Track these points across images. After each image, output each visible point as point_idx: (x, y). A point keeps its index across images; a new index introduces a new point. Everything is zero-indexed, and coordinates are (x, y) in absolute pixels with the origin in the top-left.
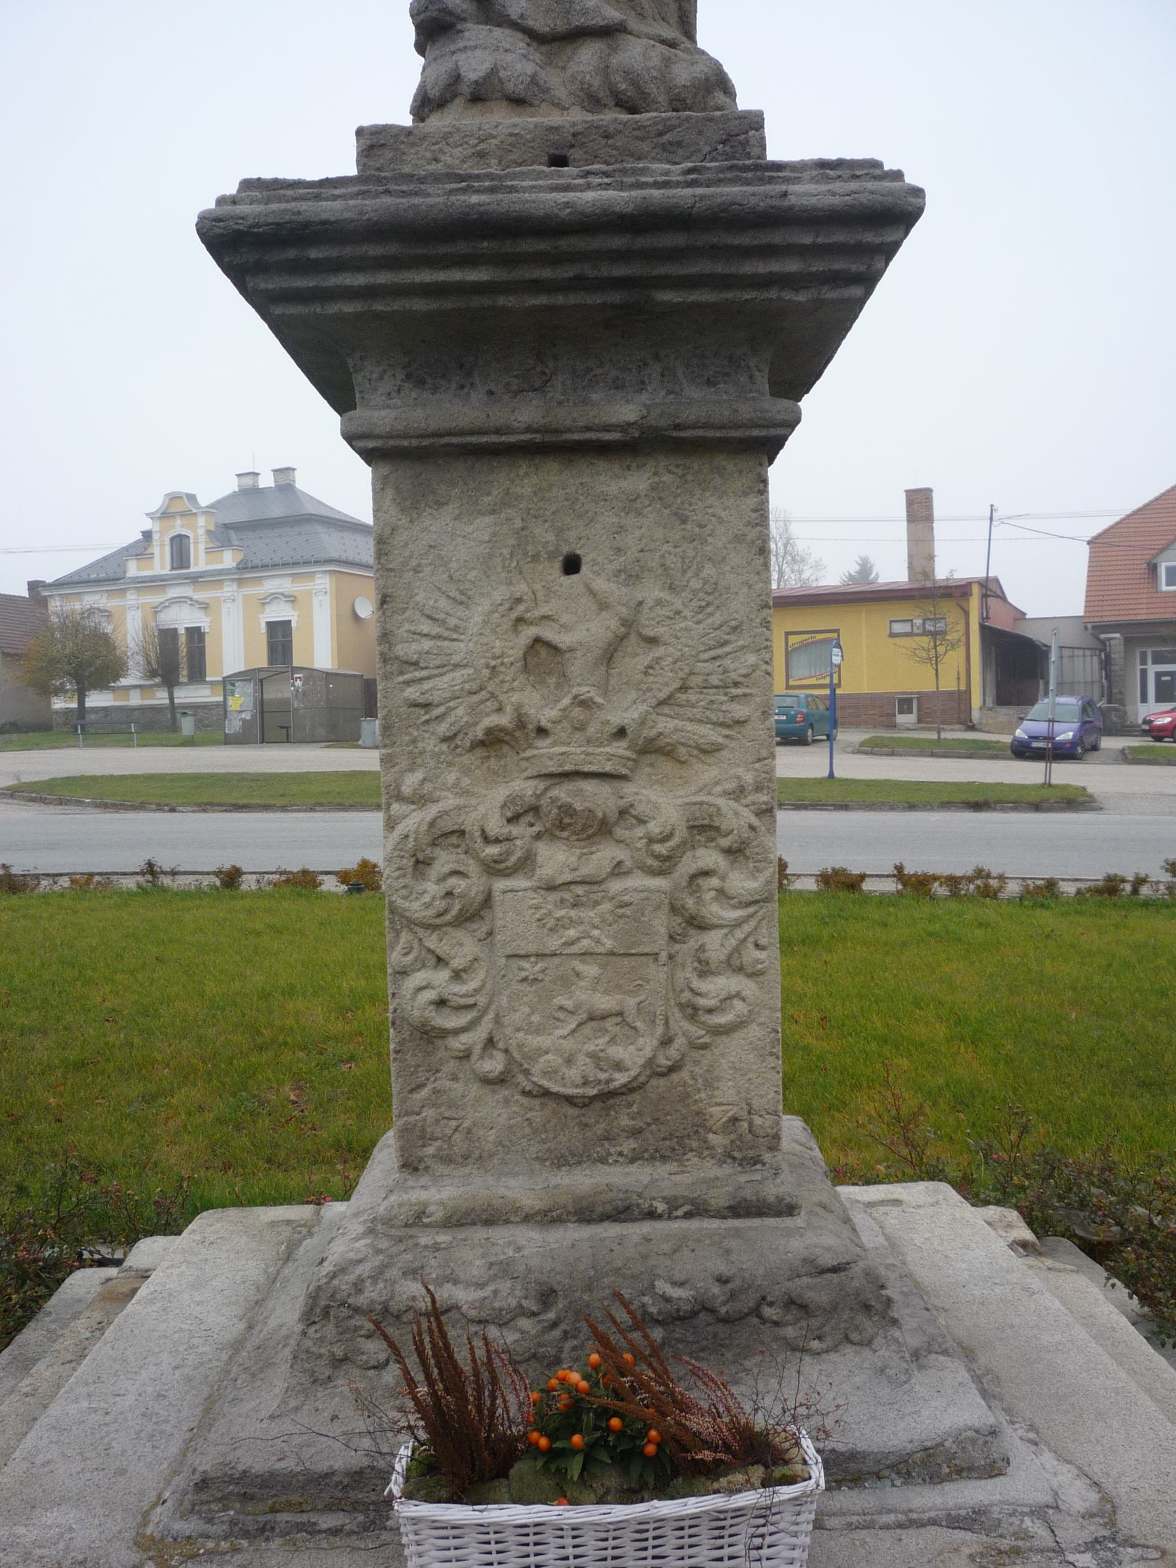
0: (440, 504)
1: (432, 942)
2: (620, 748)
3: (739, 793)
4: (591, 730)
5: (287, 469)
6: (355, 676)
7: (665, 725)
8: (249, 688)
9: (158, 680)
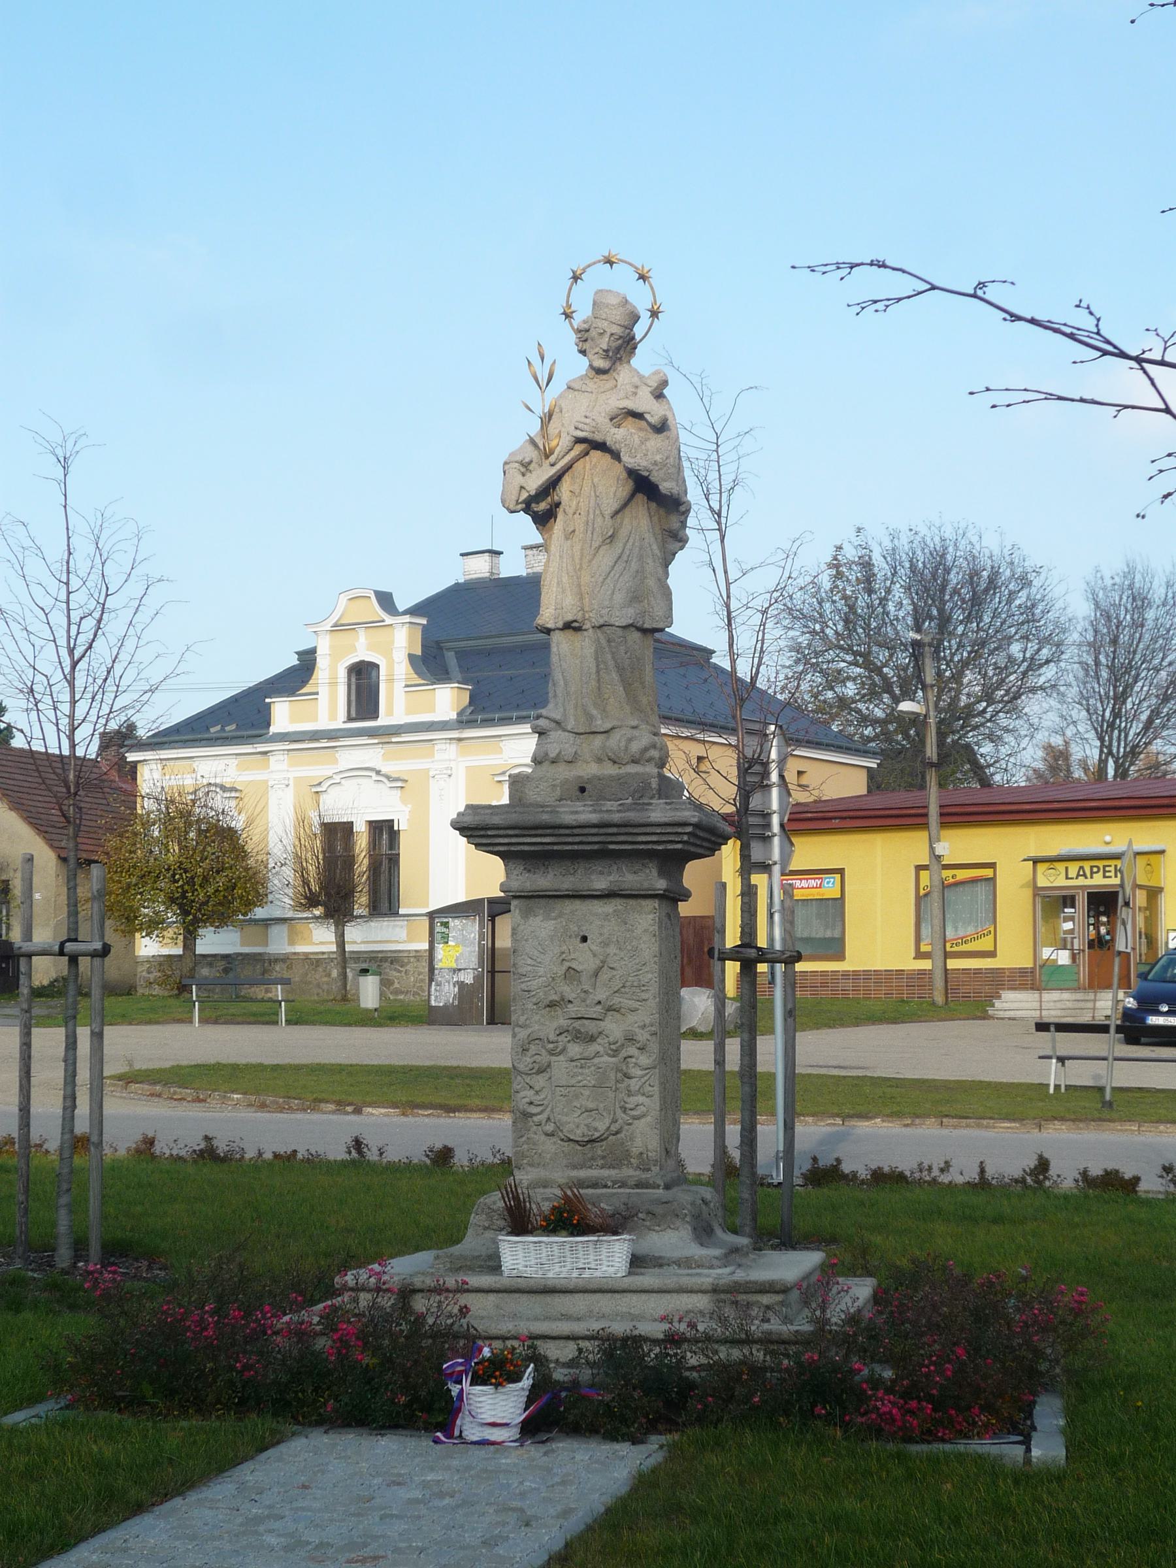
0: (535, 916)
2: (599, 1008)
7: (616, 1000)
9: (89, 749)
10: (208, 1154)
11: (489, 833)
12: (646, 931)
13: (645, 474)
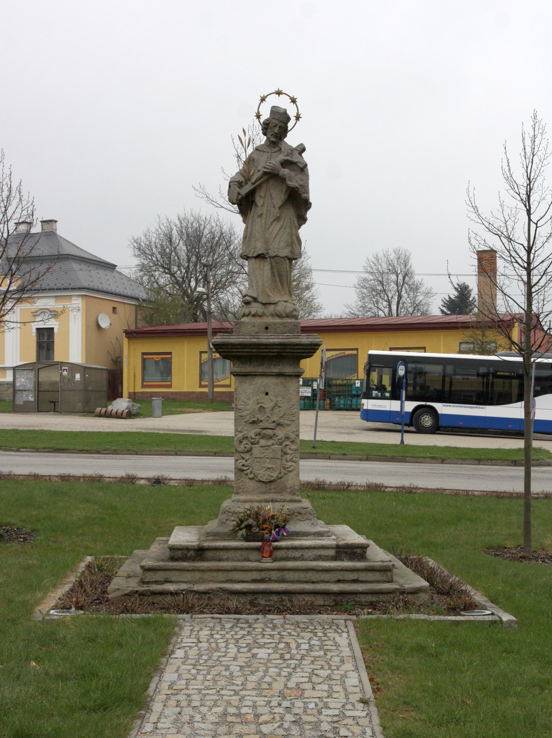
1: (242, 455)
2: (274, 424)
3: (293, 432)
4: (269, 421)
5: (51, 221)
6: (102, 369)
7: (281, 421)
8: (31, 375)
10: (64, 478)
12: (294, 390)
13: (297, 190)
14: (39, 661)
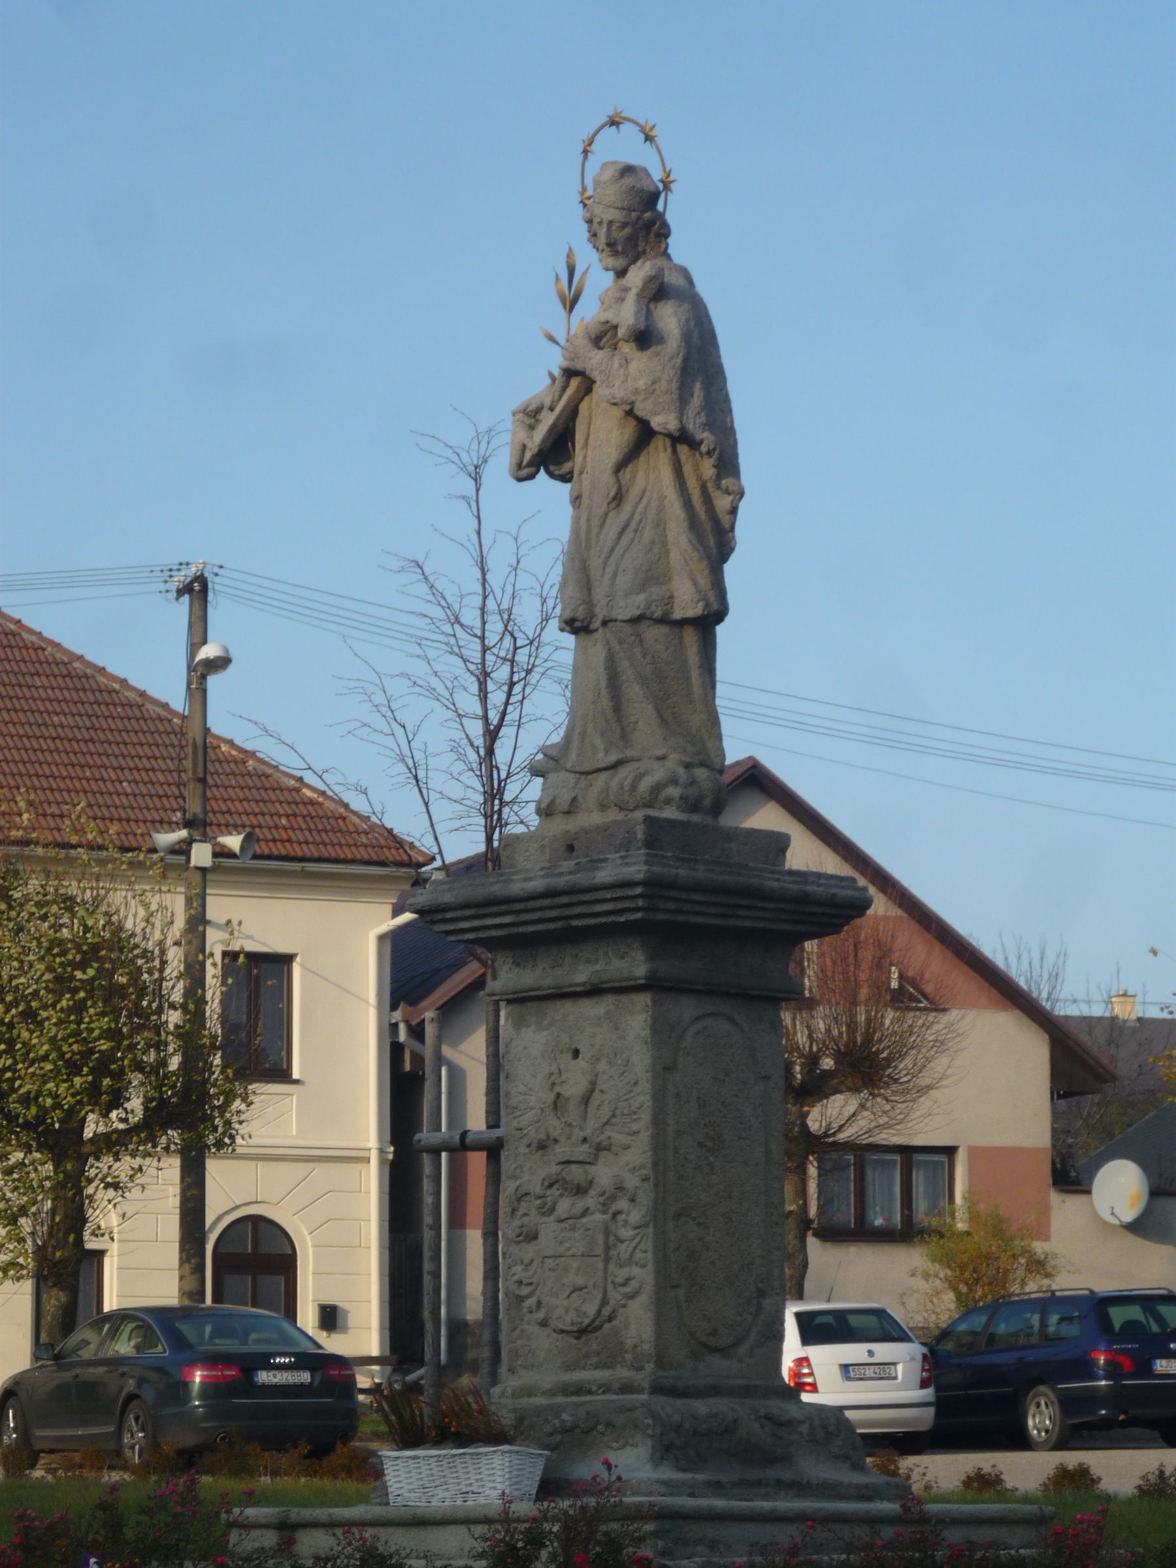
0: (528, 1026)
2: (585, 1148)
11: (448, 915)
14: (91, 954)
